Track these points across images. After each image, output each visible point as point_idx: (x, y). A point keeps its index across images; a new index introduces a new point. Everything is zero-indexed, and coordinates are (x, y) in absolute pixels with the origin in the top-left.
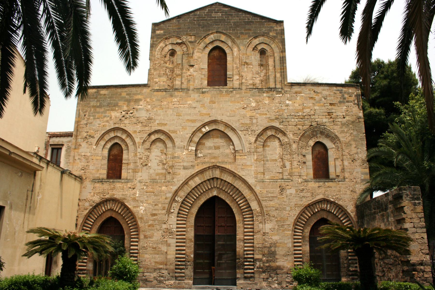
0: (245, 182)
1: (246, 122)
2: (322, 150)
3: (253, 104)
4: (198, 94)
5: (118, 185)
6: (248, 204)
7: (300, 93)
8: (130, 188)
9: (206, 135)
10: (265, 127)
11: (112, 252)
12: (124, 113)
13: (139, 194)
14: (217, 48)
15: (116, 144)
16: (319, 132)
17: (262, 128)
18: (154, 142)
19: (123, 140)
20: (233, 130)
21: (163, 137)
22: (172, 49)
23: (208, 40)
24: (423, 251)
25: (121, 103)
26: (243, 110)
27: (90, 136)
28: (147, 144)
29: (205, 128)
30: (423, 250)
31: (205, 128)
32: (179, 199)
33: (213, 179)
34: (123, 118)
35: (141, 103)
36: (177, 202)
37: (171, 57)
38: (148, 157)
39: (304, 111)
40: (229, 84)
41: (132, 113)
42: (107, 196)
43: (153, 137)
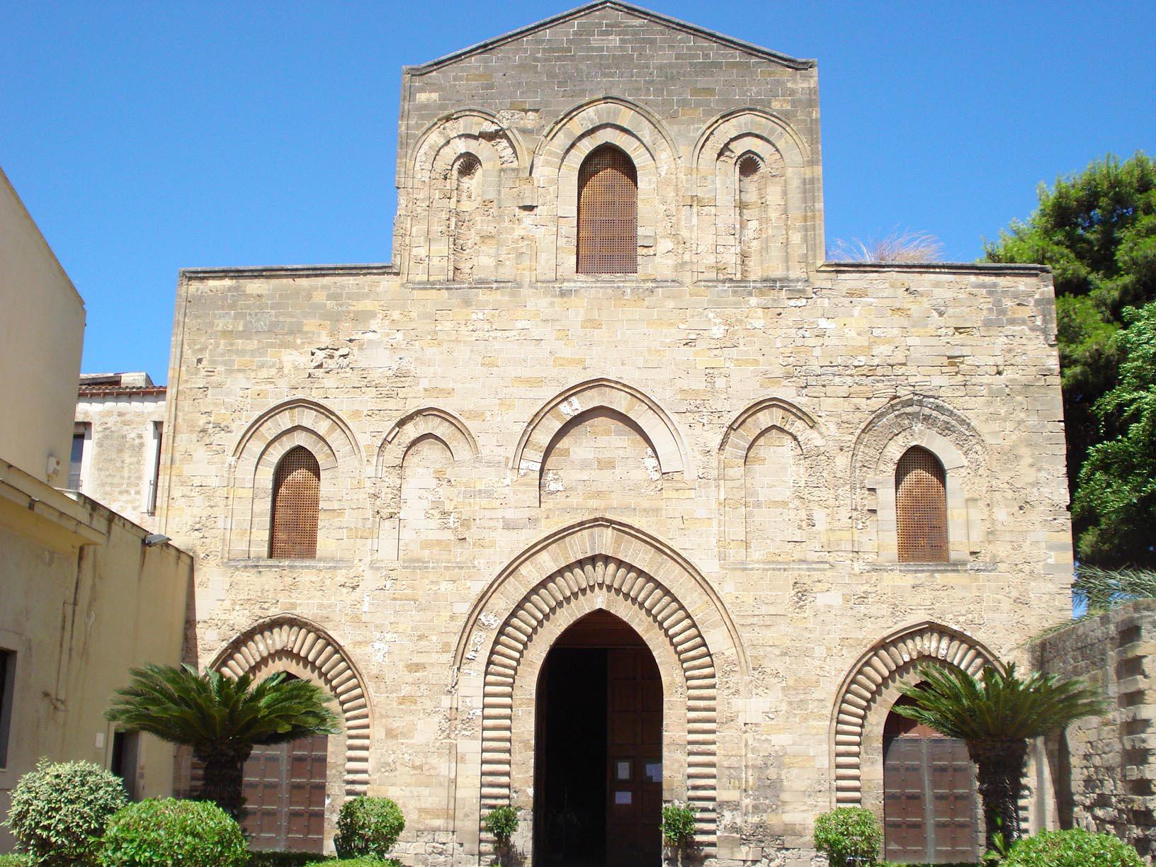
4: (549, 299)
5: (306, 574)
15: (299, 449)
20: (655, 408)
21: (442, 430)
25: (310, 324)
27: (217, 426)
34: (320, 372)
40: (646, 267)
43: (411, 431)
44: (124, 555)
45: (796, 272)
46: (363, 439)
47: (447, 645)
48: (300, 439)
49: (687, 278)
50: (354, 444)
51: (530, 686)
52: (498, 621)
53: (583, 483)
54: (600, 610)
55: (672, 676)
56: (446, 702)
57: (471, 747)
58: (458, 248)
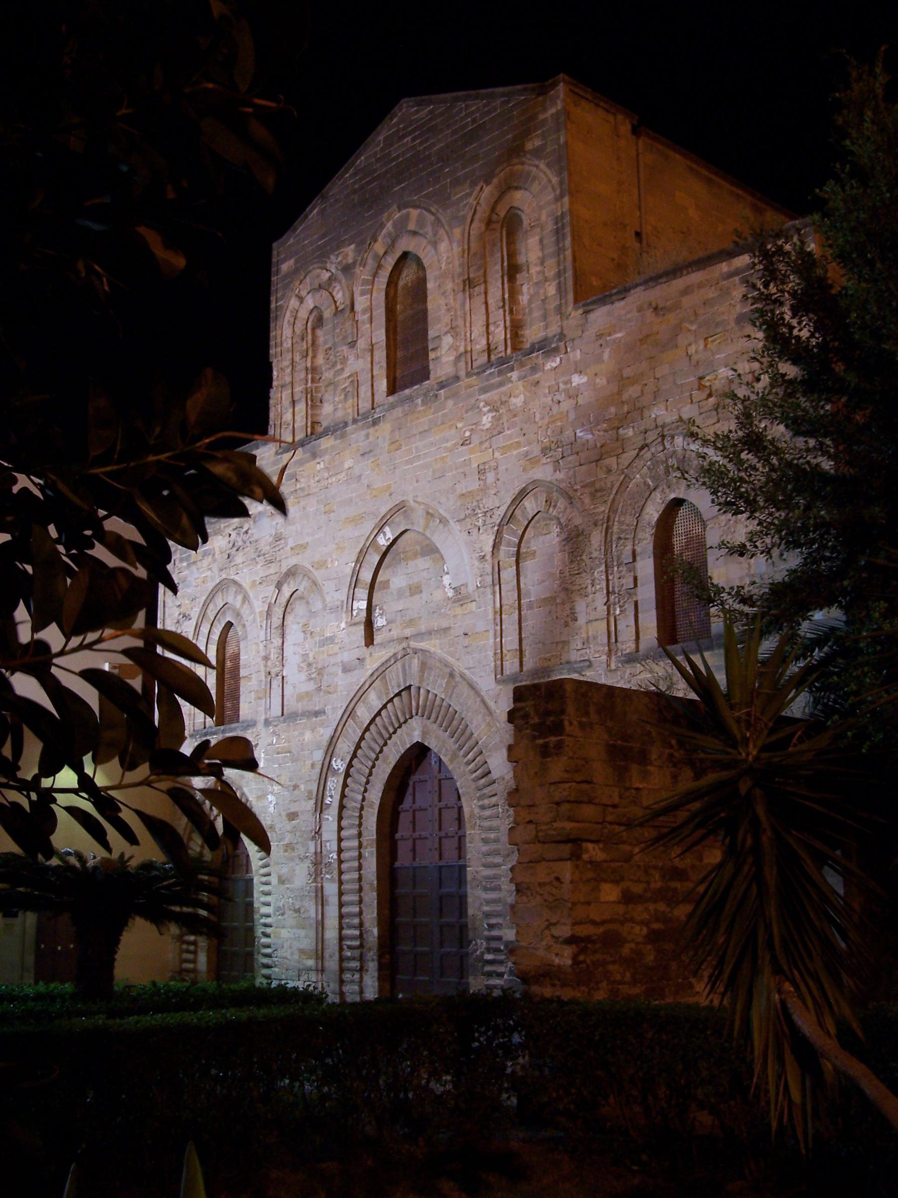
1: (469, 489)
4: (364, 433)
10: (517, 492)
13: (266, 760)
23: (379, 247)
24: (556, 931)
26: (464, 448)
30: (555, 924)
39: (625, 396)
44: (617, 691)
47: (310, 792)
51: (372, 827)
52: (344, 765)
53: (399, 614)
54: (418, 742)
55: (471, 807)
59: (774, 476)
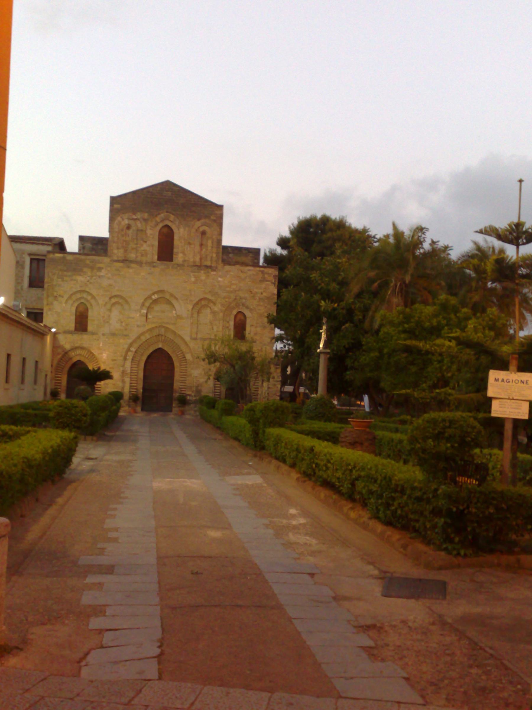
0: (183, 340)
2: (242, 318)
3: (193, 279)
5: (85, 336)
6: (184, 355)
7: (230, 271)
8: (95, 339)
9: (155, 301)
11: (403, 233)
12: (88, 278)
14: (167, 226)
15: (82, 303)
16: (241, 304)
17: (197, 299)
18: (114, 304)
19: (88, 301)
20: (177, 299)
21: (121, 301)
22: (129, 224)
23: (158, 219)
25: (85, 270)
27: (60, 296)
28: (108, 306)
29: (155, 296)
31: (155, 296)
32: (133, 349)
33: (159, 335)
34: (88, 283)
35: (103, 271)
36: (132, 351)
37: (127, 231)
38: (109, 316)
40: (175, 261)
41: (95, 279)
42: (77, 345)
43: (113, 300)
45: (214, 265)
46: (101, 302)
48: (83, 301)
49: (186, 264)
50: (98, 304)
56: (121, 369)
57: (128, 380)
58: (126, 251)
59: (490, 323)
